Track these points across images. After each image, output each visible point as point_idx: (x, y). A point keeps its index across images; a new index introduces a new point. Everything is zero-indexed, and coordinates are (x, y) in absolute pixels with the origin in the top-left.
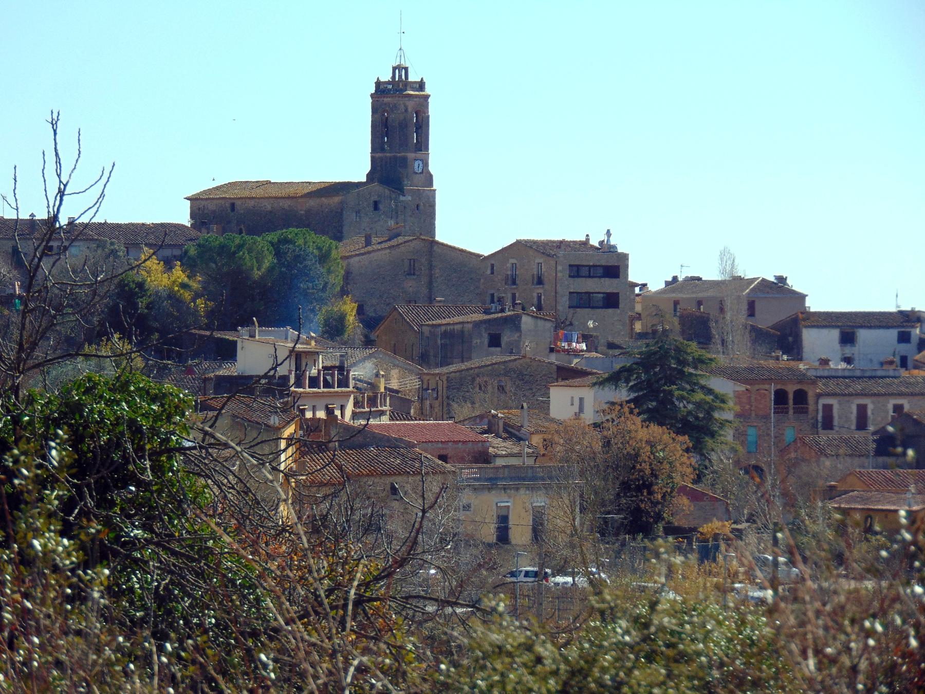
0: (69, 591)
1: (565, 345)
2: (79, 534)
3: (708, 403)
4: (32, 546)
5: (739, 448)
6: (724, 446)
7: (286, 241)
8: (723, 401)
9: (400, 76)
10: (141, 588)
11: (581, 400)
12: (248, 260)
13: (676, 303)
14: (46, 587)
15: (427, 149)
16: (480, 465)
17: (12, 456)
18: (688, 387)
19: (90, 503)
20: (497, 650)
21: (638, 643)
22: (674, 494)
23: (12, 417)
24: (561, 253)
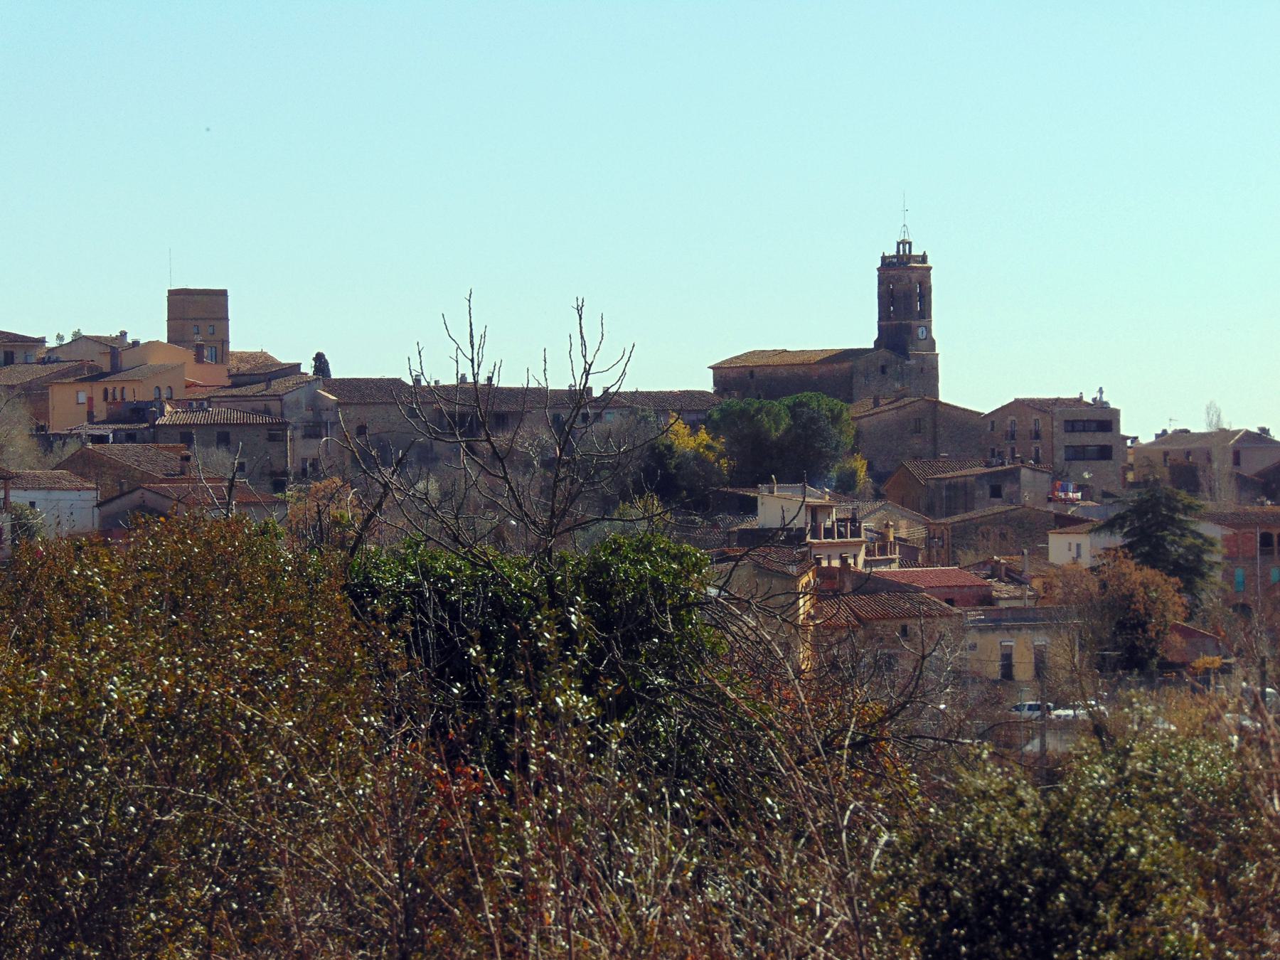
0: (589, 743)
1: (1062, 495)
2: (597, 691)
3: (1197, 546)
4: (555, 703)
5: (1229, 588)
6: (1213, 586)
7: (801, 404)
8: (1212, 544)
9: (904, 251)
10: (664, 731)
11: (1078, 546)
12: (766, 422)
13: (1166, 454)
14: (568, 740)
15: (930, 316)
16: (984, 607)
17: (536, 621)
18: (1179, 532)
19: (618, 654)
20: (981, 795)
21: (1113, 787)
22: (1167, 631)
23: (546, 577)
24: (1057, 410)
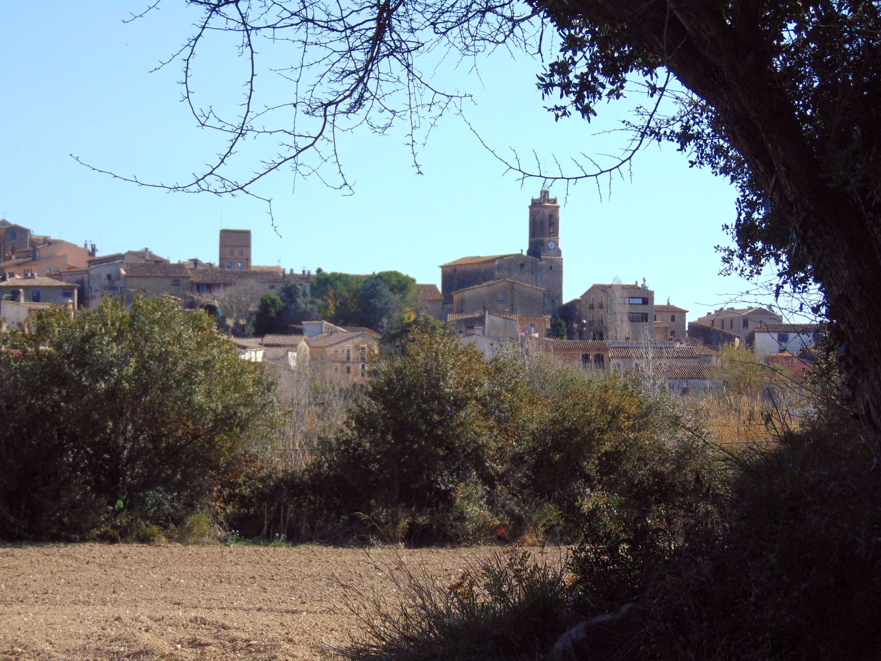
0: (318, 483)
